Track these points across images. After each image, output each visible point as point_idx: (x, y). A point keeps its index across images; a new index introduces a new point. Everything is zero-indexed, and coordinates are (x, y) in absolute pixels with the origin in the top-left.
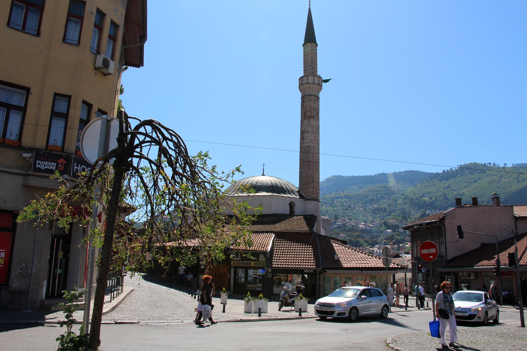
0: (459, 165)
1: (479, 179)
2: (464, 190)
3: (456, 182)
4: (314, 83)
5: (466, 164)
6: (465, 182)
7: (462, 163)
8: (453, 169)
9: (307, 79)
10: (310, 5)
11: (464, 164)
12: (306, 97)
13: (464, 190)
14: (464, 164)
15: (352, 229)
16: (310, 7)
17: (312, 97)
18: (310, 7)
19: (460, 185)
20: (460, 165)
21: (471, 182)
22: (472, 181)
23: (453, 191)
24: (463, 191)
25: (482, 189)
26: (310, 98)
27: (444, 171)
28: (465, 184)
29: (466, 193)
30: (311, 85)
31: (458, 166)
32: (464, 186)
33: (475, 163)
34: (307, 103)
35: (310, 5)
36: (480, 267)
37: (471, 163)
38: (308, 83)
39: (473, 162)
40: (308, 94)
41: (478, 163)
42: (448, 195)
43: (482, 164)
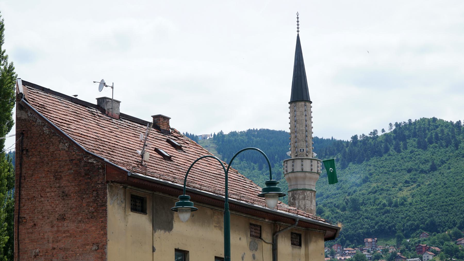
0: (393, 123)
1: (443, 162)
2: (405, 193)
3: (385, 170)
4: (311, 172)
5: (413, 121)
6: (409, 171)
7: (403, 119)
8: (380, 134)
9: (302, 165)
10: (298, 31)
11: (407, 122)
12: (299, 191)
13: (405, 193)
14: (407, 122)
15: (20, 164)
16: (298, 35)
17: (308, 192)
18: (298, 35)
19: (394, 177)
20: (397, 125)
21: (422, 171)
22: (427, 167)
23: (376, 195)
24: (401, 195)
25: (449, 190)
26: (306, 195)
27: (355, 138)
28: (407, 177)
29: (410, 200)
30: (307, 174)
31: (391, 124)
32: (407, 182)
33: (434, 119)
34: (300, 202)
35: (298, 31)
36: (202, 191)
37: (423, 120)
38: (302, 171)
39: (430, 116)
40: (302, 187)
41: (441, 121)
42: (363, 204)
43: (451, 123)
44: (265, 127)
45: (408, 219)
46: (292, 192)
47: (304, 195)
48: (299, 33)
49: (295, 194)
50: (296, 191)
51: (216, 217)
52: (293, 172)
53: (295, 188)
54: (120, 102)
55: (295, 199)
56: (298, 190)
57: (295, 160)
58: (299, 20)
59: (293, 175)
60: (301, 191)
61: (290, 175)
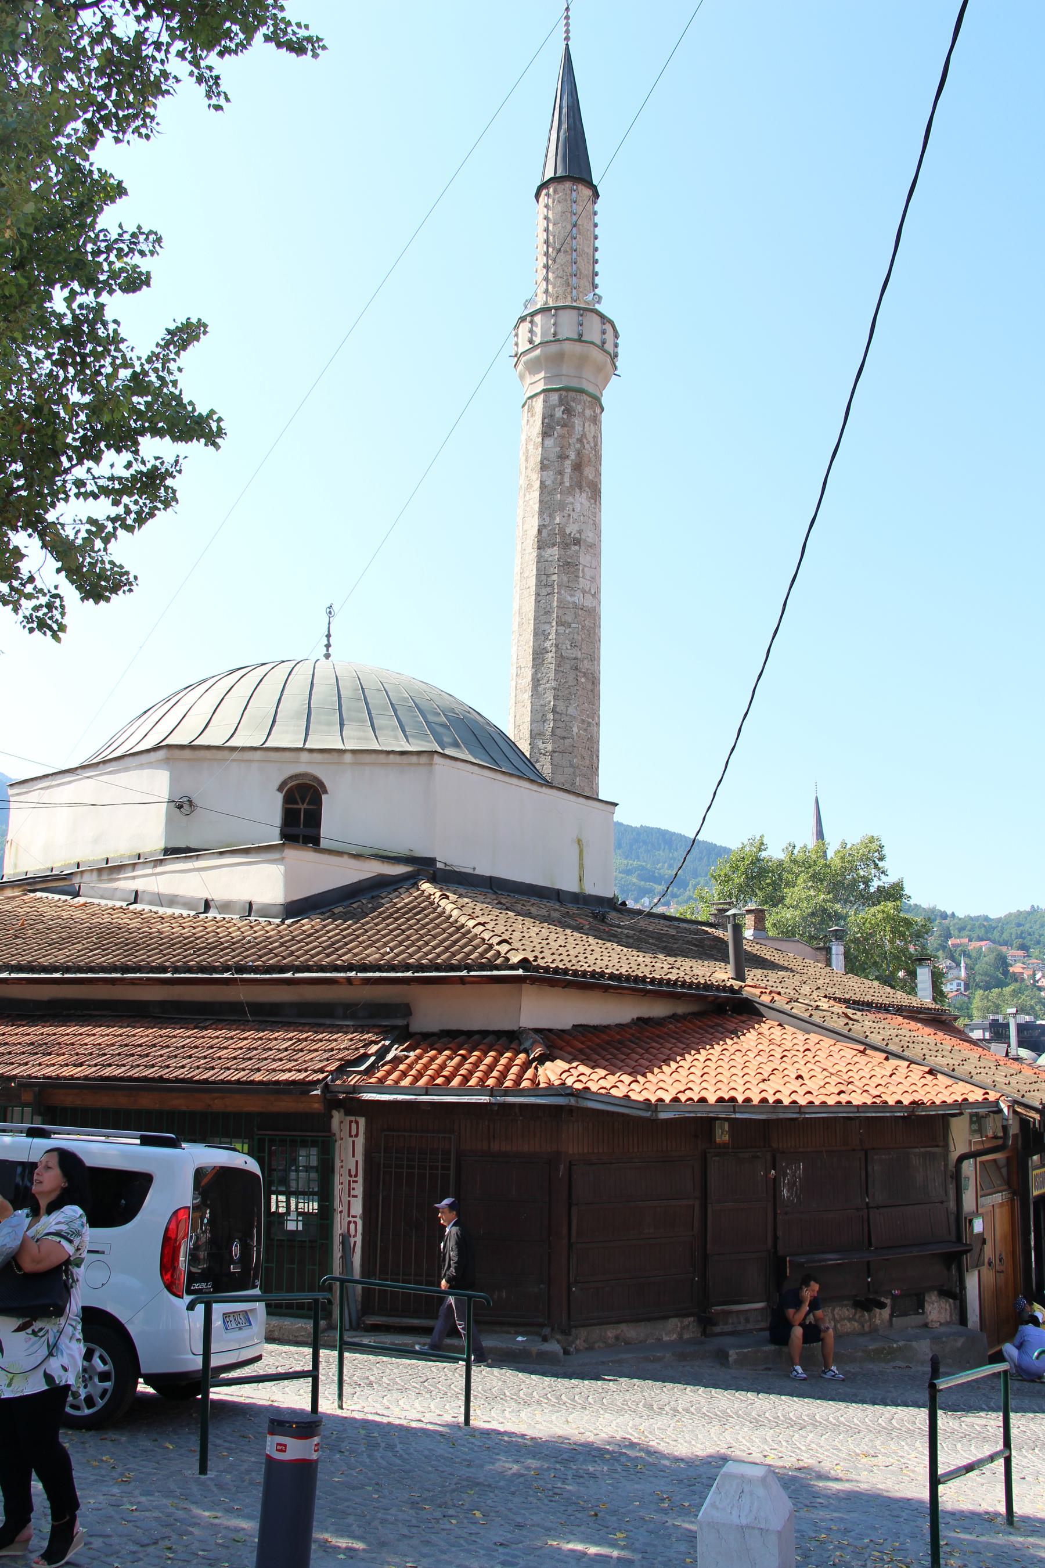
10: (567, 39)
12: (585, 397)
44: (109, 1310)
45: (105, 445)
46: (564, 393)
47: (594, 412)
48: (325, 652)
49: (573, 401)
50: (574, 393)
51: (609, 1341)
52: (580, 339)
53: (574, 384)
54: (616, 805)
55: (573, 413)
56: (582, 391)
57: (589, 313)
58: (330, 652)
59: (578, 347)
60: (589, 399)
61: (567, 346)
